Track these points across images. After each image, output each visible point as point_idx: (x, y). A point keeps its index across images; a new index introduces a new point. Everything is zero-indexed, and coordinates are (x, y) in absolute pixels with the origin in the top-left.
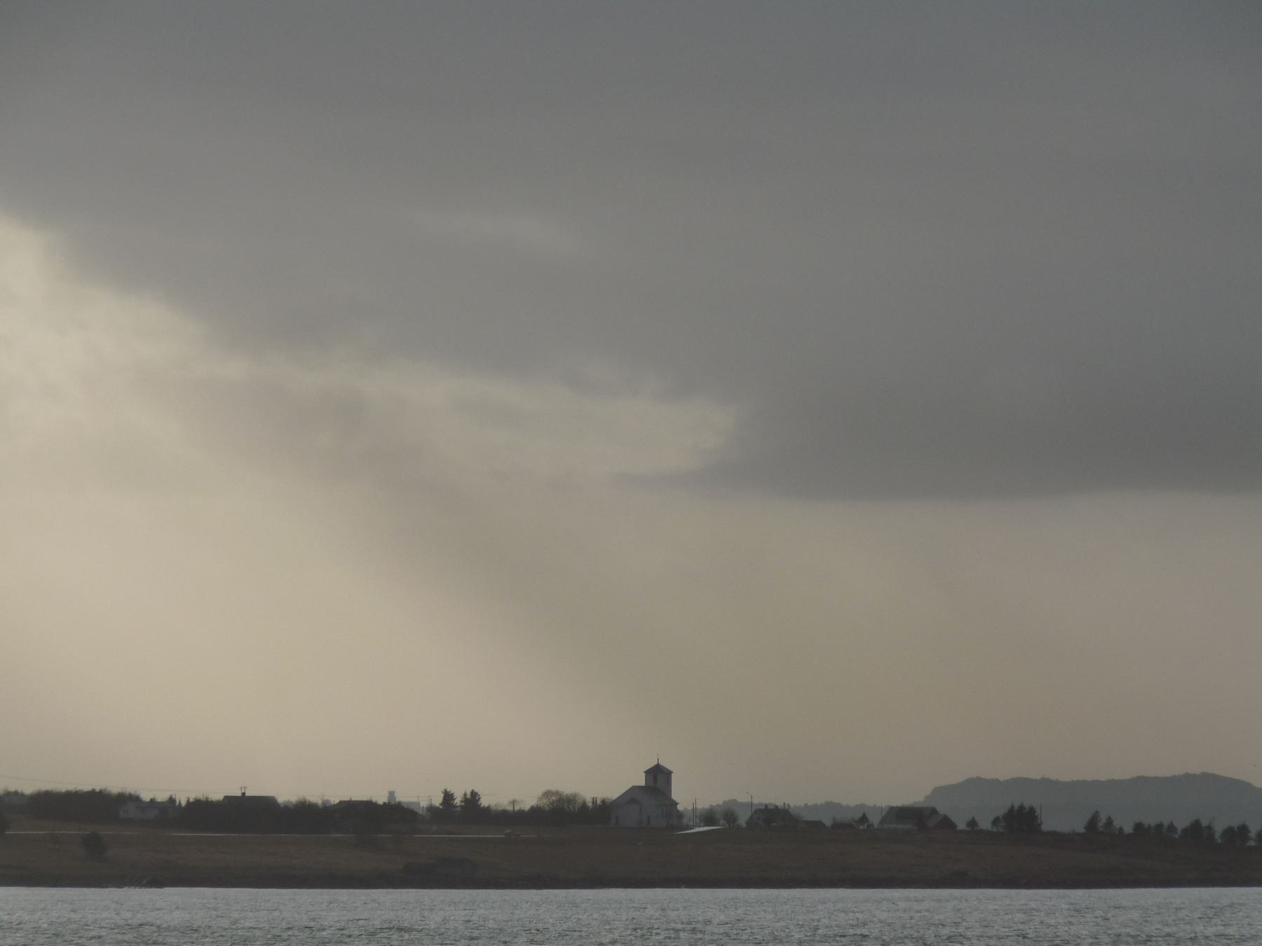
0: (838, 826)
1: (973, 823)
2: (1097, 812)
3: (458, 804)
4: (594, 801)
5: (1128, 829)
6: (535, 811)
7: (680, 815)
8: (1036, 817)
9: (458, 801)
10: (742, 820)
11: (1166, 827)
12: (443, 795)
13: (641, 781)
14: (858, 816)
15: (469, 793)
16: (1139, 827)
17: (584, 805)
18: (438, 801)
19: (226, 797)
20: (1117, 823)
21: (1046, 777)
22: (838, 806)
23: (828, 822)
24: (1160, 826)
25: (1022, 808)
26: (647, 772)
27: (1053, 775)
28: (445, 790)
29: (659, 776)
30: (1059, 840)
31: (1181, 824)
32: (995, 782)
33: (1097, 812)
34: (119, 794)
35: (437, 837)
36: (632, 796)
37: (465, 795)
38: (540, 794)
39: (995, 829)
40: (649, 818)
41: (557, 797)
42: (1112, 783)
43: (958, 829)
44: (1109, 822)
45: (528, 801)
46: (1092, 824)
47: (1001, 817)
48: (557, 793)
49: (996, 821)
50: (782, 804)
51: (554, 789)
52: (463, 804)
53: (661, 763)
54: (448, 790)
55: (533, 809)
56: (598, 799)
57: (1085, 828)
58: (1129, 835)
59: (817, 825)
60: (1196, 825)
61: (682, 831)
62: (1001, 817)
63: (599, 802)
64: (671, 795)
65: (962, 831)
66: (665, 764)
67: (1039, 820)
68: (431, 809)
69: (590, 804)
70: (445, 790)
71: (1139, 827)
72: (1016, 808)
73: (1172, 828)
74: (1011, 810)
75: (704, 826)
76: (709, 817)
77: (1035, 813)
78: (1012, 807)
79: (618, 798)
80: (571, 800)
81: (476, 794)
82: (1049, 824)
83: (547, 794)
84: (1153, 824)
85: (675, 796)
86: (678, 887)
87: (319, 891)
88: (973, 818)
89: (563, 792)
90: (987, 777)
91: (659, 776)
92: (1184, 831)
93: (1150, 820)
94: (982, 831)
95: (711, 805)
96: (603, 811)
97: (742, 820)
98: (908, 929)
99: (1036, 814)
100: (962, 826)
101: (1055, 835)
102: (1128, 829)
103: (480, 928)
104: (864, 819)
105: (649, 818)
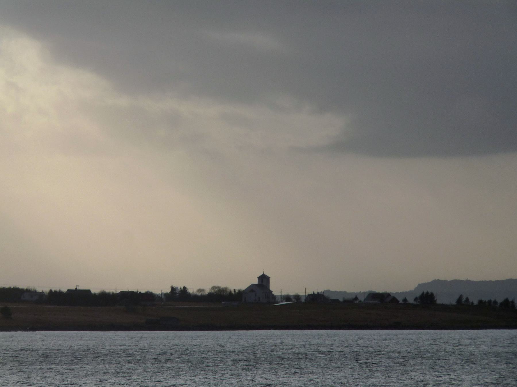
0: (345, 301)
1: (405, 300)
2: (462, 295)
3: (178, 292)
4: (235, 291)
5: (476, 303)
6: (210, 294)
7: (274, 297)
8: (434, 298)
9: (425, 293)
10: (303, 300)
11: (493, 302)
12: (171, 288)
13: (256, 282)
14: (354, 297)
15: (182, 288)
16: (480, 302)
17: (230, 292)
18: (169, 290)
19: (68, 290)
20: (471, 300)
21: (468, 279)
22: (345, 292)
23: (341, 300)
24: (490, 302)
25: (427, 293)
26: (259, 278)
27: (471, 279)
28: (172, 286)
29: (264, 279)
30: (445, 308)
31: (500, 300)
32: (445, 282)
33: (462, 295)
34: (4, 288)
35: (192, 307)
36: (252, 288)
37: (181, 288)
38: (210, 288)
39: (415, 303)
40: (259, 298)
41: (218, 289)
42: (497, 282)
43: (400, 302)
44: (467, 300)
45: (208, 289)
46: (459, 301)
47: (418, 297)
48: (218, 287)
49: (416, 299)
50: (320, 292)
51: (216, 285)
52: (180, 292)
53: (265, 273)
54: (173, 286)
55: (209, 294)
56: (237, 290)
57: (456, 302)
58: (476, 305)
59: (337, 301)
60: (506, 301)
61: (288, 304)
62: (418, 297)
63: (237, 291)
64: (269, 288)
65: (401, 304)
66: (267, 274)
67: (435, 299)
68: (166, 295)
69: (233, 293)
70: (172, 286)
71: (480, 302)
72: (425, 293)
73: (495, 302)
74: (423, 293)
75: (285, 302)
76: (287, 298)
77: (434, 295)
78: (423, 293)
79: (245, 290)
80: (224, 290)
81: (186, 288)
82: (439, 301)
83: (214, 288)
84: (487, 301)
85: (272, 288)
86: (270, 329)
87: (122, 332)
88: (406, 298)
89: (221, 287)
90: (442, 279)
91: (264, 279)
92: (501, 304)
93: (485, 299)
94: (409, 304)
95: (43, 291)
96: (239, 295)
97: (303, 300)
98: (158, 344)
99: (434, 296)
100: (401, 302)
101: (442, 305)
102: (476, 303)
103: (393, 355)
104: (356, 298)
105: (259, 298)
